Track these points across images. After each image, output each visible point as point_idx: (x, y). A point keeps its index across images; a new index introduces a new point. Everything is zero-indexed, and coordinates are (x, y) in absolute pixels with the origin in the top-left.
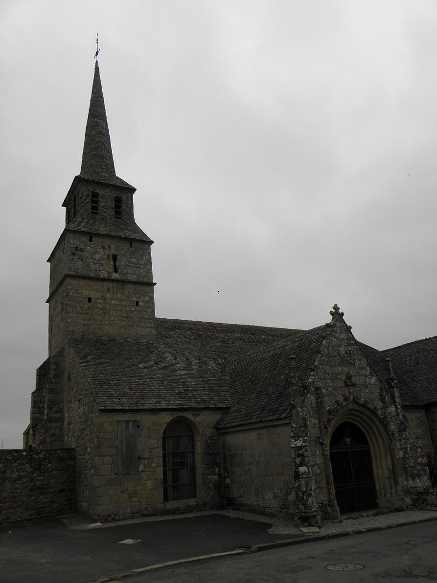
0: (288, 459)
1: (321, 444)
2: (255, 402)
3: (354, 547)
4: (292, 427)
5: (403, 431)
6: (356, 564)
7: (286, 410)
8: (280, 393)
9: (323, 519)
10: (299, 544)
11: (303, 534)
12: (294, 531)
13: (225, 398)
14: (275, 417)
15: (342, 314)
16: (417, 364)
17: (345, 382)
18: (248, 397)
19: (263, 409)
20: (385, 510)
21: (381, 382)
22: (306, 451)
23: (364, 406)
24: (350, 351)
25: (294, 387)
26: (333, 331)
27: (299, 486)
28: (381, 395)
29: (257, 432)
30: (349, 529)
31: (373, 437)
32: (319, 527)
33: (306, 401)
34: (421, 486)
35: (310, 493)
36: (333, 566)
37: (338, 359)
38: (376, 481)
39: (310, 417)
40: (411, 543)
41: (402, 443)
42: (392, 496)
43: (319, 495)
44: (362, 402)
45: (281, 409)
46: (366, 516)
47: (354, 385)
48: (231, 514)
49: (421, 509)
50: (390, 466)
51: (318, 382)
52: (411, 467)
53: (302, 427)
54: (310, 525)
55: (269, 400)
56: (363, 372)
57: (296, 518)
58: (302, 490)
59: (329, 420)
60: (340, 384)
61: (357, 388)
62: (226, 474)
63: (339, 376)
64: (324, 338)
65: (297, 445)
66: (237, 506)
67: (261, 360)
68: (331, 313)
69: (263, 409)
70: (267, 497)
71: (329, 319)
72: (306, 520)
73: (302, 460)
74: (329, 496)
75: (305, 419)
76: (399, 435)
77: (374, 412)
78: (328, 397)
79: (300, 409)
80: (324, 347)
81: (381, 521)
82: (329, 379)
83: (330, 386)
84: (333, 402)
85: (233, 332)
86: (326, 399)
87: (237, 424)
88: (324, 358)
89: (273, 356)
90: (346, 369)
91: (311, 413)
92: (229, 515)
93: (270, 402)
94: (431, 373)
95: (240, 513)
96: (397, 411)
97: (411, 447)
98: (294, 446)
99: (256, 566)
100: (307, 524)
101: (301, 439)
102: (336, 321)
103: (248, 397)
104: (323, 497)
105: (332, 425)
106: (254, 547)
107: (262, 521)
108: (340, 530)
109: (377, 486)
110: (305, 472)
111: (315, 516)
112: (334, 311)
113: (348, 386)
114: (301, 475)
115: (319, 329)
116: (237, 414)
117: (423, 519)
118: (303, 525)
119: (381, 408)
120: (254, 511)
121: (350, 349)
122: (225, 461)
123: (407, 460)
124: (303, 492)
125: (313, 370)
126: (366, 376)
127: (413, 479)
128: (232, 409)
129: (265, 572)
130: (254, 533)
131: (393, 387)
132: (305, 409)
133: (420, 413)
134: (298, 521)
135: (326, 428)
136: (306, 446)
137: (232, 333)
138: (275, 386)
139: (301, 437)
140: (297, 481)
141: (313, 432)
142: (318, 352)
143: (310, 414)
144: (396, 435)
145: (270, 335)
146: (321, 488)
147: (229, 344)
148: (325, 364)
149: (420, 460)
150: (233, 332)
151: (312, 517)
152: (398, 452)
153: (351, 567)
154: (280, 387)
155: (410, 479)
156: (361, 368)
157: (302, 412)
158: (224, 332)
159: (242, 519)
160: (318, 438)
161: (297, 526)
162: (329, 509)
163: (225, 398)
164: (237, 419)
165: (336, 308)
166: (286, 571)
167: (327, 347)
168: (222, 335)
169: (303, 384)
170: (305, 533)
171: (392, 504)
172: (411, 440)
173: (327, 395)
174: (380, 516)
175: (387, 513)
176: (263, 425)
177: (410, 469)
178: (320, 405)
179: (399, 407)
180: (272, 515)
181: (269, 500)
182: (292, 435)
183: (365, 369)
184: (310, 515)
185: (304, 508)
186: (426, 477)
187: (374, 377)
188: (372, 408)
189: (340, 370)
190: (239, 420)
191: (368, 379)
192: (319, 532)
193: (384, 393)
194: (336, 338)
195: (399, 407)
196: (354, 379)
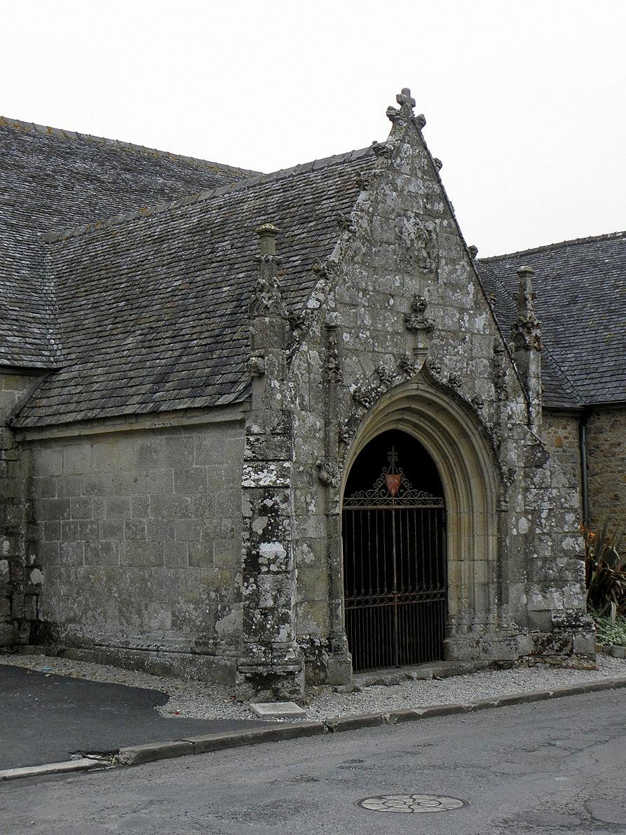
0: (227, 523)
1: (325, 484)
2: (137, 358)
3: (414, 754)
4: (249, 433)
5: (538, 467)
6: (439, 796)
7: (234, 383)
8: (218, 336)
9: (309, 682)
10: (252, 744)
11: (259, 721)
12: (231, 712)
13: (43, 342)
14: (199, 402)
15: (421, 122)
16: (574, 301)
17: (406, 321)
18: (114, 343)
19: (162, 379)
20: (468, 665)
21: (498, 329)
22: (286, 499)
23: (449, 390)
24: (429, 232)
25: (267, 320)
26: (390, 167)
27: (256, 596)
28: (495, 365)
29: (138, 442)
30: (377, 710)
31: (458, 476)
32: (302, 703)
33: (296, 361)
34: (562, 607)
35: (286, 615)
36: (376, 801)
37: (394, 251)
38: (452, 592)
39: (303, 408)
40: (558, 743)
41: (530, 497)
42: (486, 630)
43: (309, 613)
44: (445, 381)
45: (219, 379)
46: (419, 679)
47: (429, 330)
48: (43, 664)
49: (553, 666)
50: (493, 555)
51: (334, 310)
52: (545, 560)
53: (278, 434)
54: (277, 697)
55: (181, 356)
56: (458, 295)
57: (240, 678)
58: (262, 605)
59: (353, 422)
60: (392, 323)
61: (436, 341)
62: (33, 557)
63: (392, 302)
64: (361, 186)
65: (262, 483)
66: (60, 647)
67: (161, 240)
68: (392, 115)
69: (162, 379)
70: (154, 624)
71: (381, 132)
72: (266, 683)
73: (271, 524)
74: (332, 625)
75: (287, 413)
76: (526, 476)
77: (470, 408)
78: (357, 356)
79: (278, 384)
80: (362, 210)
81: (457, 692)
82: (364, 306)
83: (365, 328)
84: (369, 374)
85: (69, 154)
86: (350, 362)
87: (79, 417)
88: (358, 244)
89: (196, 230)
90: (413, 284)
91: (307, 398)
92: (39, 669)
93: (184, 359)
94: (606, 328)
95: (70, 663)
96: (529, 412)
97: (549, 510)
98: (253, 485)
99: (151, 802)
100: (268, 693)
101: (272, 467)
102: (403, 141)
103: (114, 343)
104: (316, 627)
105: (359, 434)
106: (127, 752)
107: (136, 685)
108: (355, 712)
109: (453, 606)
110: (277, 557)
111: (291, 673)
112: (398, 107)
113: (412, 331)
114: (262, 565)
115: (347, 159)
116: (80, 388)
117: (563, 688)
118: (256, 696)
119: (492, 401)
120: (111, 661)
121: (431, 227)
122: (32, 522)
123: (537, 542)
124: (266, 612)
125: (324, 276)
126: (462, 310)
127: (544, 591)
128: (64, 376)
129: (183, 819)
130: (122, 714)
131: (527, 348)
132: (291, 384)
133: (565, 428)
134: (245, 686)
135: (341, 441)
136: (287, 487)
137: (66, 159)
138: (203, 316)
139: (273, 461)
140: (252, 580)
141: (307, 449)
142: (344, 225)
143: (302, 397)
144: (519, 476)
145: (179, 178)
146: (312, 602)
147: (56, 187)
148: (358, 263)
149: (568, 543)
150: (69, 154)
151: (285, 678)
152: (517, 521)
153: (429, 805)
154: (218, 320)
155: (536, 588)
156: (454, 286)
157: (282, 392)
158: (43, 152)
159: (77, 680)
160: (319, 467)
161: (236, 700)
162: (326, 657)
163: (43, 342)
164: (78, 402)
165: (405, 99)
166: (246, 814)
167: (368, 213)
168: (35, 160)
169: (291, 313)
170: (264, 716)
171: (485, 651)
172: (555, 491)
173: (355, 352)
174: (454, 679)
175: (470, 672)
176: (158, 423)
177: (540, 563)
178: (332, 375)
179: (536, 401)
180: (166, 671)
181: (160, 630)
182: (248, 453)
183: (463, 288)
184: (279, 670)
185: (264, 652)
186: (578, 585)
187: (484, 316)
188: (468, 398)
189: (397, 284)
190: (83, 406)
191: (466, 318)
192: (303, 715)
193: (504, 361)
194: (395, 190)
195: (536, 401)
196: (429, 314)
